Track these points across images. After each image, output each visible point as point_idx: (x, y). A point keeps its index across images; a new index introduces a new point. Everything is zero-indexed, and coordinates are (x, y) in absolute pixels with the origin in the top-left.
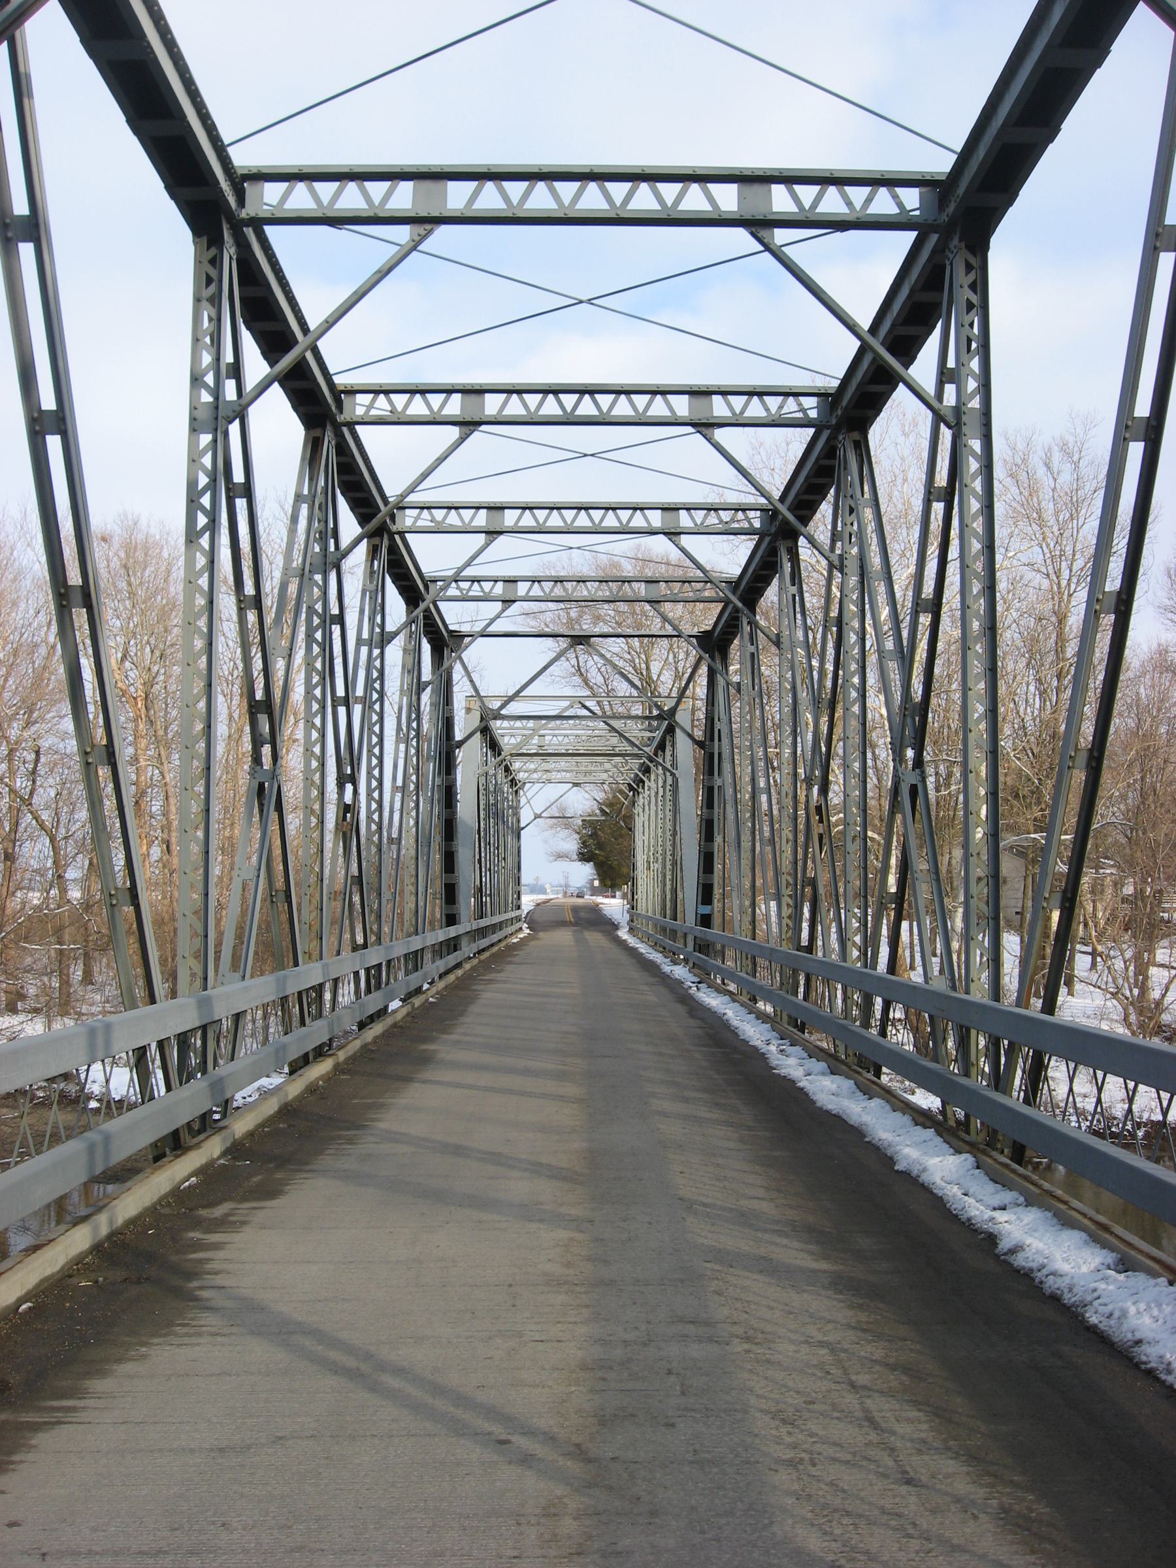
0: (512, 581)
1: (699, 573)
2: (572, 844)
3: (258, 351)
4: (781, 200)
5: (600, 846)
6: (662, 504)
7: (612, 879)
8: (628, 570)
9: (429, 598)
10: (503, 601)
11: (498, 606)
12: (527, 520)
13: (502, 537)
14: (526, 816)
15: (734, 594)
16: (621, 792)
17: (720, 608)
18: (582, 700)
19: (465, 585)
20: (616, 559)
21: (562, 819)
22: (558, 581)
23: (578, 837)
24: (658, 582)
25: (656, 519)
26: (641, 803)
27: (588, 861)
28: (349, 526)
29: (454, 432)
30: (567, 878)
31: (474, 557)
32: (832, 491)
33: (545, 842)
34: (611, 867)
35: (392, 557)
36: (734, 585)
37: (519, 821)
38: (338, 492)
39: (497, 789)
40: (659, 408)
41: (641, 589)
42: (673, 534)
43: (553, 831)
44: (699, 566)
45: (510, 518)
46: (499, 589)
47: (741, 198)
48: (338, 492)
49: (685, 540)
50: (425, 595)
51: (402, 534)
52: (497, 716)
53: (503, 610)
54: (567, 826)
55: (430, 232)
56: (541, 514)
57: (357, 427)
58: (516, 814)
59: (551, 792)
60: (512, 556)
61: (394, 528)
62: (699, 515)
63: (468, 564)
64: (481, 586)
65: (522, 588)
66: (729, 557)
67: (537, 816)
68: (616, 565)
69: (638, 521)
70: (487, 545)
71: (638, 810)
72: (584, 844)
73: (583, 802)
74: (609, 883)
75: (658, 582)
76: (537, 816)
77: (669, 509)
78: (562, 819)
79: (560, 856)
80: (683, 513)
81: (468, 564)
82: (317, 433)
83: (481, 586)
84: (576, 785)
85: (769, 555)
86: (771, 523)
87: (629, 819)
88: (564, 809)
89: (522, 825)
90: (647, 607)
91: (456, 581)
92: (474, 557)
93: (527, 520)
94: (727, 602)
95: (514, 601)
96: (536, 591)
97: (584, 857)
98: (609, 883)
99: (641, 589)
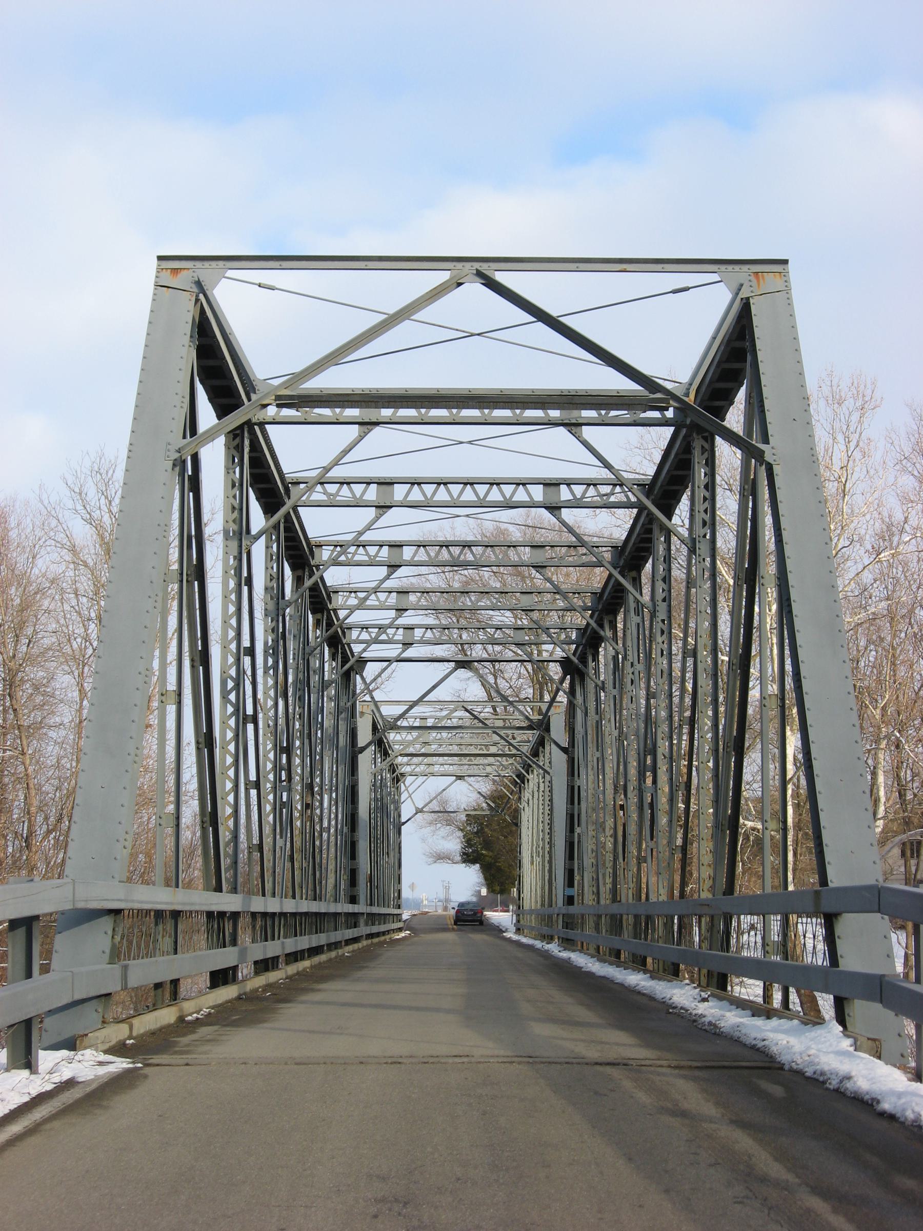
0: (386, 483)
1: (605, 474)
2: (453, 844)
3: (206, 397)
4: (565, 494)
5: (487, 844)
6: (544, 479)
7: (501, 884)
8: (516, 535)
9: (289, 504)
10: (388, 566)
11: (393, 613)
12: (416, 495)
13: (378, 429)
14: (406, 811)
15: (648, 497)
16: (506, 786)
17: (669, 436)
18: (484, 267)
19: (332, 488)
20: (503, 526)
21: (443, 814)
22: (446, 545)
23: (460, 834)
24: (544, 546)
25: (538, 493)
26: (526, 799)
27: (473, 862)
28: (258, 519)
29: (355, 430)
30: (447, 889)
31: (346, 452)
32: (650, 561)
33: (423, 840)
34: (499, 869)
35: (254, 455)
36: (648, 488)
37: (400, 816)
38: (197, 379)
39: (383, 785)
40: (521, 495)
41: (526, 554)
42: (554, 509)
43: (432, 828)
44: (607, 465)
45: (399, 492)
46: (372, 493)
47: (545, 494)
48: (197, 379)
49: (565, 513)
50: (286, 500)
51: (335, 610)
52: (394, 727)
53: (377, 518)
54: (449, 823)
55: (370, 431)
56: (429, 489)
57: (267, 426)
58: (398, 809)
59: (435, 784)
60: (401, 525)
61: (330, 607)
62: (578, 490)
63: (336, 462)
64: (366, 551)
65: (407, 553)
66: (614, 525)
67: (419, 811)
68: (503, 532)
69: (521, 495)
70: (361, 438)
71: (524, 804)
72: (468, 842)
73: (467, 795)
74: (498, 888)
75: (544, 546)
76: (419, 811)
77: (551, 485)
78: (443, 814)
79: (441, 857)
80: (563, 488)
81: (336, 462)
82: (300, 573)
83: (366, 551)
84: (460, 778)
85: (677, 468)
86: (583, 637)
87: (516, 815)
88: (444, 802)
89: (403, 820)
90: (533, 571)
91: (322, 483)
92: (346, 452)
93: (416, 495)
94: (641, 508)
95: (391, 507)
96: (422, 555)
97: (468, 858)
98: (498, 888)
99: (526, 554)
